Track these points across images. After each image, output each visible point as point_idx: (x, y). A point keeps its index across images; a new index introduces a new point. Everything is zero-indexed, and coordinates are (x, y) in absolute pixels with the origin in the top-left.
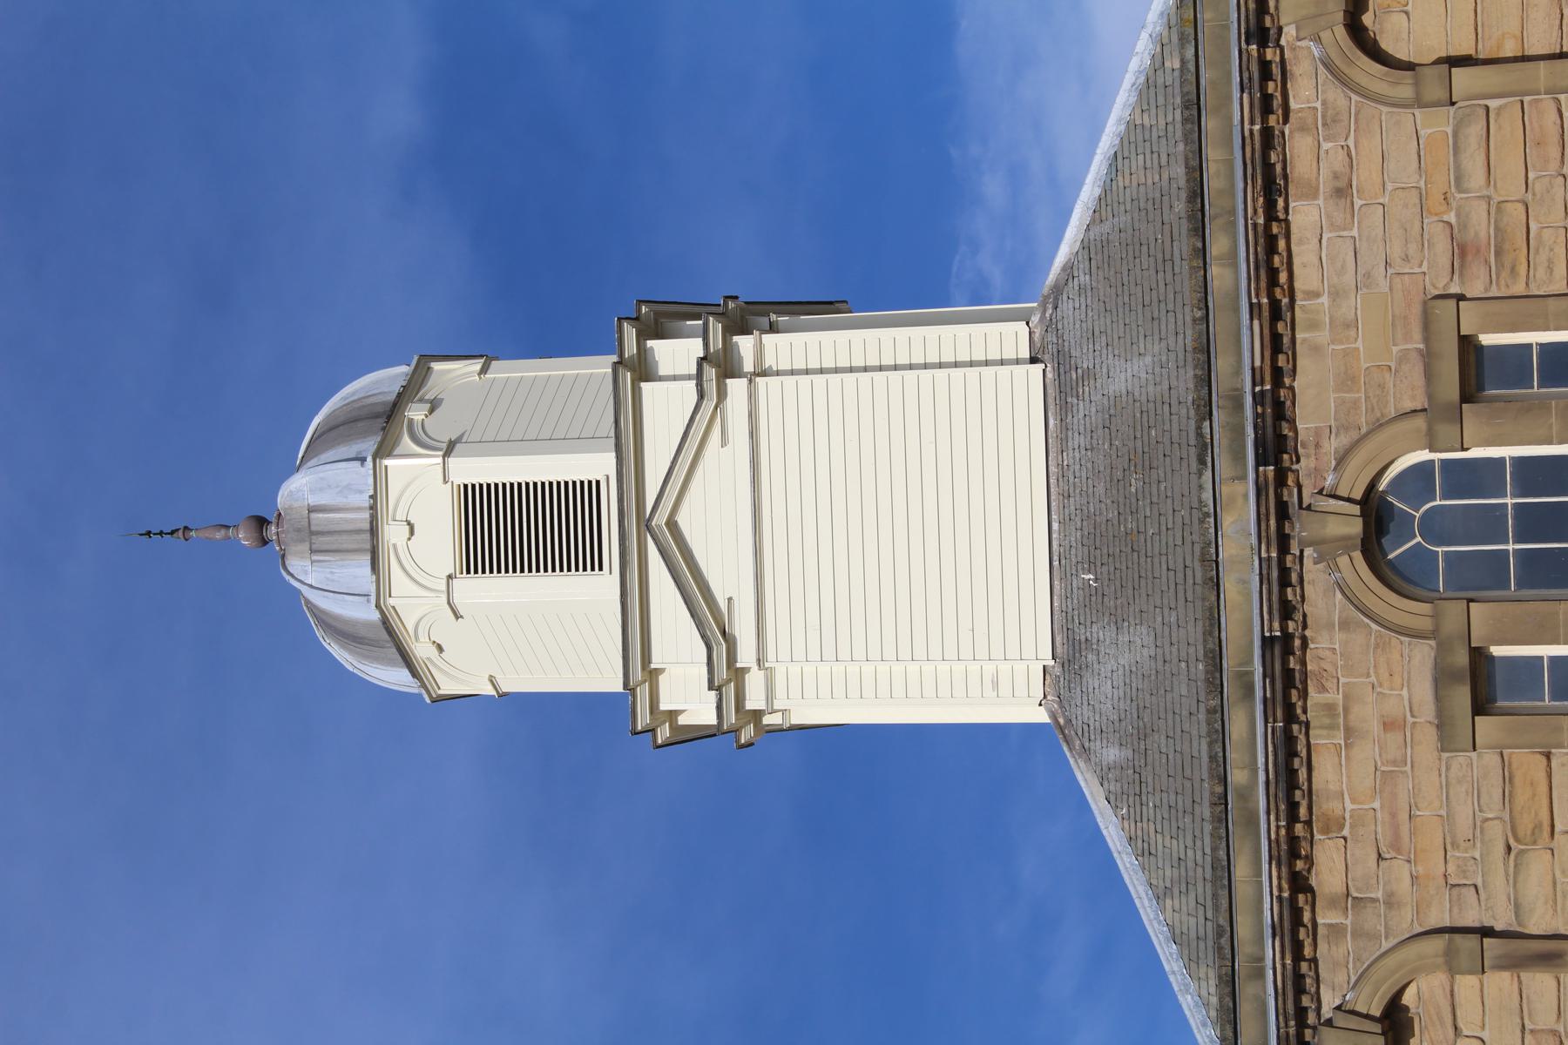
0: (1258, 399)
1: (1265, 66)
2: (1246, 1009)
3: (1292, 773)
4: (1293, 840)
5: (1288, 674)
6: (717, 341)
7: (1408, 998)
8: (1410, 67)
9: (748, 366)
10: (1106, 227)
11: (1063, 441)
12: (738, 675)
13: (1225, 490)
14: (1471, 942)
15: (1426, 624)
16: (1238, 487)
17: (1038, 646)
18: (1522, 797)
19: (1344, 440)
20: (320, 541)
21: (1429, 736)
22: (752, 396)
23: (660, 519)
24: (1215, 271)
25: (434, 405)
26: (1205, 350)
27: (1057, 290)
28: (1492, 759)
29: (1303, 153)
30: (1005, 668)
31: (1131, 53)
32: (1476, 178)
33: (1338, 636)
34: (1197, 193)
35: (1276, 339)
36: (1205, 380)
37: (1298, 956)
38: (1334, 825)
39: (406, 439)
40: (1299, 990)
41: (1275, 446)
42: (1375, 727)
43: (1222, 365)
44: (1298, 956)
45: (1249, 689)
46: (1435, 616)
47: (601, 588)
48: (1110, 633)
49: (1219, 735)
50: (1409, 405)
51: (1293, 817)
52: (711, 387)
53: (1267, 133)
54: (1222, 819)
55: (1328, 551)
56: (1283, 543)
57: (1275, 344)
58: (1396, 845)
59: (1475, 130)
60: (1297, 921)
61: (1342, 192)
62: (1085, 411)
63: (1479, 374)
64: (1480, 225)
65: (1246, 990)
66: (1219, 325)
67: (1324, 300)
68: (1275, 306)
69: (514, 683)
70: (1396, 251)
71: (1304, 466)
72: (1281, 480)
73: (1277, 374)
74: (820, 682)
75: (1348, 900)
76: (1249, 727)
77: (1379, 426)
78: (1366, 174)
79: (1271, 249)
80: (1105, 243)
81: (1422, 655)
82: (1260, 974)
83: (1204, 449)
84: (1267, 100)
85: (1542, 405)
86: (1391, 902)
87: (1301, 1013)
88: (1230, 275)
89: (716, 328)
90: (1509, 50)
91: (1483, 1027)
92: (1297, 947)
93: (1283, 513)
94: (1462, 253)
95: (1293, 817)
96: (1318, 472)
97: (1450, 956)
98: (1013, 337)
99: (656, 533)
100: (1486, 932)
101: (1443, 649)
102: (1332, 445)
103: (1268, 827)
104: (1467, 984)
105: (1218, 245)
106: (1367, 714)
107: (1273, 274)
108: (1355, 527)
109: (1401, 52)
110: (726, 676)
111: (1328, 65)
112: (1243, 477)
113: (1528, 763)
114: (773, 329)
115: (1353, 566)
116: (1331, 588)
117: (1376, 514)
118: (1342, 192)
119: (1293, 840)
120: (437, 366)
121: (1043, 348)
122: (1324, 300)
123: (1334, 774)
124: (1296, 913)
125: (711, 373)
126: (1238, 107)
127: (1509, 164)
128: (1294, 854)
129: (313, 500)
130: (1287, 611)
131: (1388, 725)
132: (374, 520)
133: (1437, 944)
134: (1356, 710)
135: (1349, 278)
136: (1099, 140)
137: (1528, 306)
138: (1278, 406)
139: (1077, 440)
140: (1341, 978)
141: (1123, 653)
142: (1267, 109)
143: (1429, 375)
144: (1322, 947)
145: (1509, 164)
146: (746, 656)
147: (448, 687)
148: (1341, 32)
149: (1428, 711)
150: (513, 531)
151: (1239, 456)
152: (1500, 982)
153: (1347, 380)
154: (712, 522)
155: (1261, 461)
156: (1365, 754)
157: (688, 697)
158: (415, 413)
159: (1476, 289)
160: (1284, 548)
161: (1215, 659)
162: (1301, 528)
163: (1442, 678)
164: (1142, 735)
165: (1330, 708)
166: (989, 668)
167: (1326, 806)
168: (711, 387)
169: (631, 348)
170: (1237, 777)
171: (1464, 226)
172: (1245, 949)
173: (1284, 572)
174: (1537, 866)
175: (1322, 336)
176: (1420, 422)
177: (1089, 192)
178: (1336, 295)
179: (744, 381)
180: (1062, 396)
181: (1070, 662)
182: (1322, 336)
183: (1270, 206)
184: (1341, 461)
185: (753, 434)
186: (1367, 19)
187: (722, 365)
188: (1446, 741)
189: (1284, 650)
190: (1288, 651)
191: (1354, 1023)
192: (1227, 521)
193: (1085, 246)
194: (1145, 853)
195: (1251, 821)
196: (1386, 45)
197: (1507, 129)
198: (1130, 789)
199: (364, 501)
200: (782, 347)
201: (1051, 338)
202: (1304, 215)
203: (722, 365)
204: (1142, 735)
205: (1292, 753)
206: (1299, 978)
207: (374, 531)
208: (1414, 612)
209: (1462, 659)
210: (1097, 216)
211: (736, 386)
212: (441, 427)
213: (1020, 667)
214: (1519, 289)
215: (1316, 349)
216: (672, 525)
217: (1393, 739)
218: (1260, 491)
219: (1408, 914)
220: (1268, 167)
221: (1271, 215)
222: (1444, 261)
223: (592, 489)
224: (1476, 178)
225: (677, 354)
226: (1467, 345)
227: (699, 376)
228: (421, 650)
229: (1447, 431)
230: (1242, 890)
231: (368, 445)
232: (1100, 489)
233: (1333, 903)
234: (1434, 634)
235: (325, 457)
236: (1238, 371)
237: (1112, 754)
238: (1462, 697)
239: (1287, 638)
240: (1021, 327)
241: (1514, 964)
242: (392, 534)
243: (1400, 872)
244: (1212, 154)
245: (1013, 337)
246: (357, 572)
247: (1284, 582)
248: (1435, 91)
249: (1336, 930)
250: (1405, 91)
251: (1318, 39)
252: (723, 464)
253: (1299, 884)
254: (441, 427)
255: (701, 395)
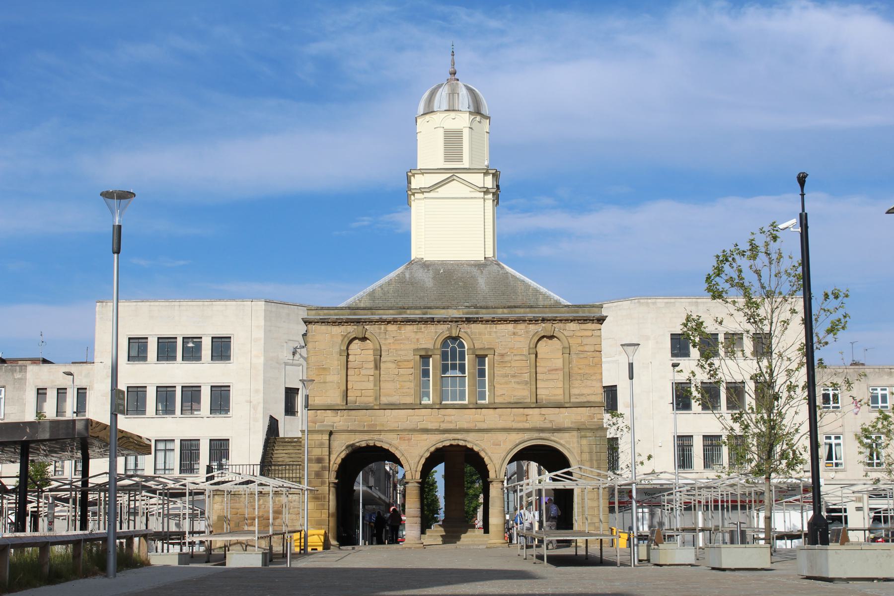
11: (471, 265)
12: (423, 193)
17: (428, 257)
18: (406, 363)
27: (499, 265)
28: (412, 358)
29: (522, 326)
38: (400, 329)
41: (468, 321)
43: (484, 311)
49: (416, 308)
54: (401, 308)
55: (450, 329)
59: (524, 358)
61: (514, 334)
62: (475, 271)
63: (481, 358)
64: (507, 358)
65: (369, 312)
66: (491, 310)
69: (419, 137)
76: (417, 314)
77: (472, 340)
78: (517, 338)
80: (507, 278)
82: (372, 314)
86: (386, 339)
89: (494, 191)
94: (502, 355)
98: (490, 254)
99: (453, 174)
101: (432, 350)
102: (469, 331)
104: (371, 352)
105: (505, 311)
106: (419, 336)
108: (454, 335)
110: (422, 191)
115: (447, 334)
116: (443, 330)
118: (514, 334)
123: (409, 329)
126: (530, 316)
127: (517, 364)
131: (418, 339)
136: (433, 586)
137: (492, 367)
139: (469, 268)
141: (426, 279)
143: (481, 349)
145: (517, 364)
150: (452, 139)
152: (372, 358)
153: (480, 334)
154: (453, 188)
156: (413, 335)
157: (418, 182)
158: (478, 118)
161: (430, 308)
162: (453, 324)
163: (426, 349)
167: (403, 327)
170: (408, 311)
172: (377, 312)
174: (393, 366)
177: (518, 275)
178: (496, 332)
180: (479, 266)
181: (426, 265)
195: (400, 314)
197: (524, 364)
198: (401, 279)
200: (489, 204)
202: (510, 327)
208: (438, 345)
209: (430, 353)
210: (513, 276)
212: (475, 125)
223: (460, 160)
225: (489, 182)
226: (486, 356)
228: (427, 117)
229: (471, 352)
230: (387, 312)
231: (472, 109)
237: (407, 276)
238: (423, 353)
240: (491, 255)
241: (375, 360)
242: (453, 114)
243: (391, 341)
244: (522, 310)
245: (490, 254)
246: (445, 107)
248: (531, 351)
252: (466, 191)
253: (389, 322)
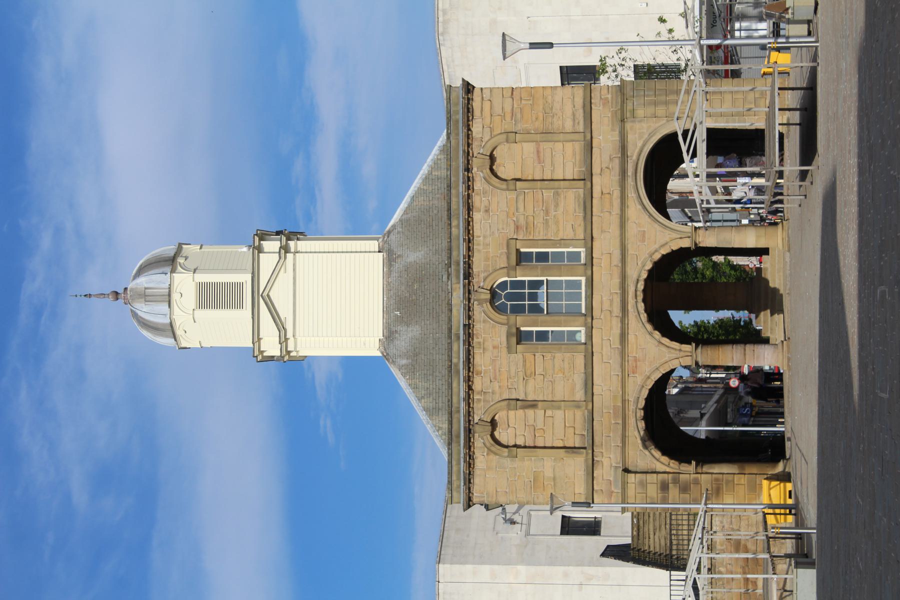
0: (464, 263)
1: (469, 177)
2: (454, 421)
3: (469, 359)
4: (469, 377)
5: (469, 334)
6: (284, 242)
7: (496, 418)
8: (505, 180)
9: (292, 250)
10: (409, 216)
12: (286, 339)
13: (454, 286)
14: (514, 402)
15: (506, 322)
16: (457, 286)
17: (378, 332)
18: (528, 365)
19: (486, 274)
20: (148, 298)
21: (505, 350)
22: (294, 259)
23: (265, 294)
24: (453, 229)
25: (186, 258)
26: (450, 249)
27: (389, 232)
28: (520, 356)
29: (476, 200)
30: (367, 339)
31: (421, 169)
32: (521, 209)
33: (482, 324)
34: (449, 209)
35: (469, 247)
36: (450, 258)
37: (469, 407)
38: (479, 373)
39: (179, 268)
40: (469, 415)
41: (468, 275)
42: (491, 348)
43: (454, 253)
44: (469, 407)
45: (459, 338)
46: (508, 319)
47: (246, 313)
48: (405, 328)
49: (450, 349)
50: (502, 266)
51: (469, 371)
52: (283, 256)
53: (468, 195)
54: (450, 371)
55: (481, 302)
56: (469, 300)
57: (469, 249)
58: (495, 378)
59: (522, 197)
60: (469, 398)
62: (398, 266)
64: (522, 222)
65: (455, 416)
66: (454, 244)
67: (481, 238)
68: (469, 239)
69: (206, 344)
70: (501, 227)
71: (475, 281)
72: (469, 284)
73: (469, 256)
74: (309, 344)
75: (482, 392)
76: (459, 349)
78: (493, 207)
79: (469, 225)
80: (408, 220)
81: (504, 329)
82: (459, 412)
83: (449, 275)
84: (469, 186)
85: (537, 267)
86: (493, 393)
87: (469, 421)
88: (458, 230)
89: (284, 238)
90: (530, 178)
91: (781, 136)
92: (469, 404)
93: (469, 293)
94: (517, 228)
95: (469, 371)
96: (478, 282)
97: (509, 405)
98: (374, 245)
99: (260, 297)
100: (518, 400)
102: (482, 275)
103: (462, 373)
104: (512, 413)
106: (489, 345)
107: (469, 231)
108: (488, 296)
109: (503, 177)
110: (283, 341)
111: (485, 179)
112: (459, 283)
113: (529, 356)
114: (298, 239)
115: (487, 307)
117: (494, 294)
118: (487, 211)
119: (469, 377)
120: (184, 246)
121: (383, 248)
122: (481, 238)
123: (480, 360)
124: (469, 395)
125: (283, 251)
126: (462, 188)
128: (469, 380)
129: (146, 286)
130: (469, 318)
131: (494, 347)
132: (170, 291)
133: (506, 403)
134: (486, 344)
135: (488, 233)
137: (534, 242)
138: (469, 265)
139: (394, 274)
140: (480, 412)
141: (408, 335)
142: (469, 189)
143: (508, 258)
144: (475, 404)
146: (290, 334)
147: (184, 344)
148: (488, 171)
149: (505, 344)
150: (212, 297)
151: (458, 277)
152: (520, 412)
153: (487, 259)
154: (280, 295)
155: (465, 279)
156: (488, 354)
157: (271, 347)
159: (520, 237)
160: (469, 302)
162: (473, 297)
164: (416, 355)
165: (479, 343)
166: (363, 339)
167: (477, 368)
168: (283, 256)
169: (257, 244)
170: (455, 360)
171: (518, 221)
173: (469, 307)
174: (531, 383)
175: (481, 247)
176: (505, 270)
178: (485, 237)
179: (292, 255)
180: (390, 260)
181: (389, 336)
182: (481, 247)
183: (469, 213)
184: (485, 280)
185: (294, 270)
186: (494, 167)
187: (285, 249)
188: (509, 350)
189: (468, 327)
190: (469, 328)
191: (483, 423)
192: (454, 294)
193: (401, 220)
194: (415, 388)
195: (458, 372)
196: (499, 174)
197: (529, 197)
198: (409, 371)
199: (167, 286)
200: (302, 245)
201: (386, 245)
202: (477, 216)
203: (285, 249)
204: (416, 355)
205: (469, 354)
206: (469, 412)
207: (169, 295)
208: (502, 318)
209: (514, 330)
210: (406, 212)
211: (290, 256)
213: (372, 339)
214: (531, 238)
215: (479, 251)
216: (268, 295)
217: (496, 351)
218: (464, 286)
219: (498, 395)
220: (468, 203)
221: (469, 216)
222: (513, 230)
223: (241, 285)
224: (521, 209)
225: (272, 245)
226: (518, 251)
227: (280, 252)
229: (512, 273)
230: (455, 390)
232: (403, 288)
233: (479, 393)
234: (507, 324)
235: (150, 272)
236: (459, 255)
238: (514, 340)
239: (469, 324)
240: (376, 243)
241: (524, 408)
242: (175, 296)
243: (496, 385)
244: (454, 199)
245: (374, 245)
246: (164, 307)
247: (469, 310)
249: (479, 400)
250: (504, 187)
251: (695, 269)
252: (284, 280)
253: (470, 388)
254: (190, 264)
255: (280, 258)
